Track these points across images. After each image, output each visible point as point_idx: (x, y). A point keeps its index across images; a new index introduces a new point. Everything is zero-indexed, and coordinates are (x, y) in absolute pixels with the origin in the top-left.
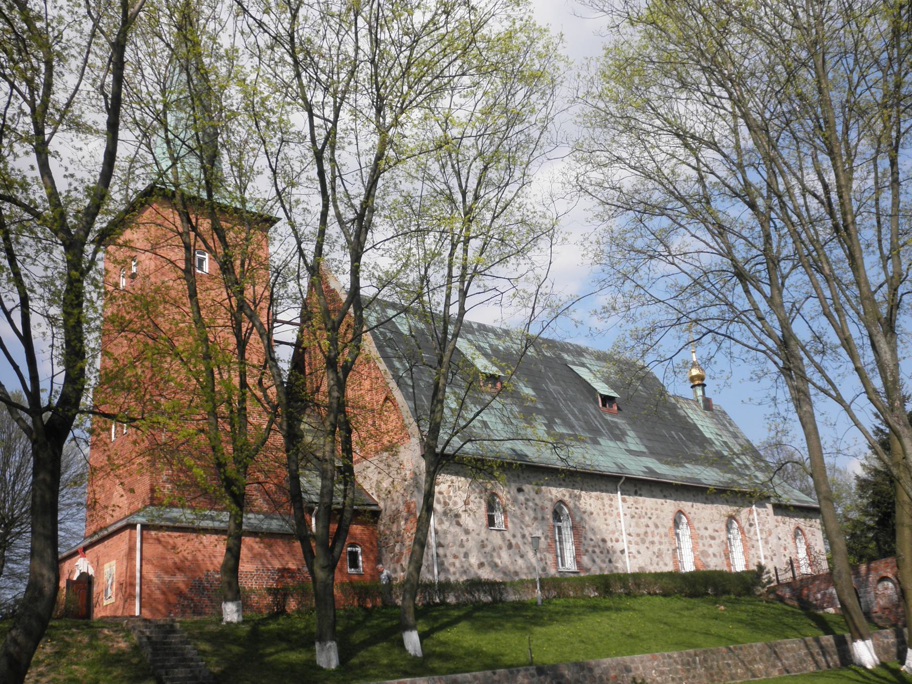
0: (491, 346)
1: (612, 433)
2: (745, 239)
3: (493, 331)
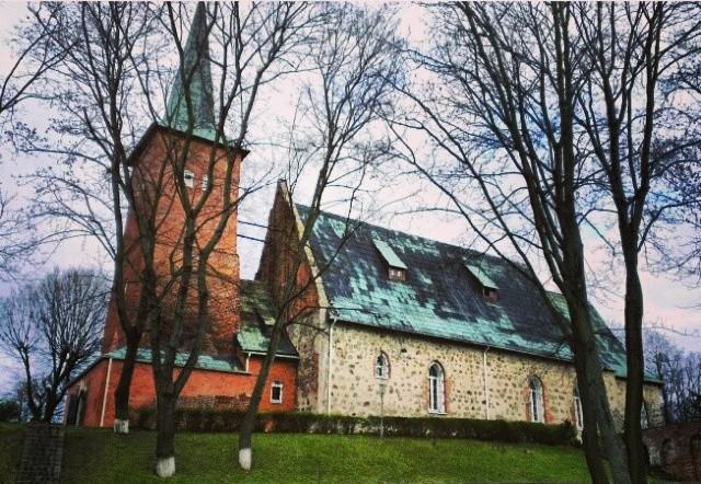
0: (406, 248)
1: (487, 314)
3: (411, 238)
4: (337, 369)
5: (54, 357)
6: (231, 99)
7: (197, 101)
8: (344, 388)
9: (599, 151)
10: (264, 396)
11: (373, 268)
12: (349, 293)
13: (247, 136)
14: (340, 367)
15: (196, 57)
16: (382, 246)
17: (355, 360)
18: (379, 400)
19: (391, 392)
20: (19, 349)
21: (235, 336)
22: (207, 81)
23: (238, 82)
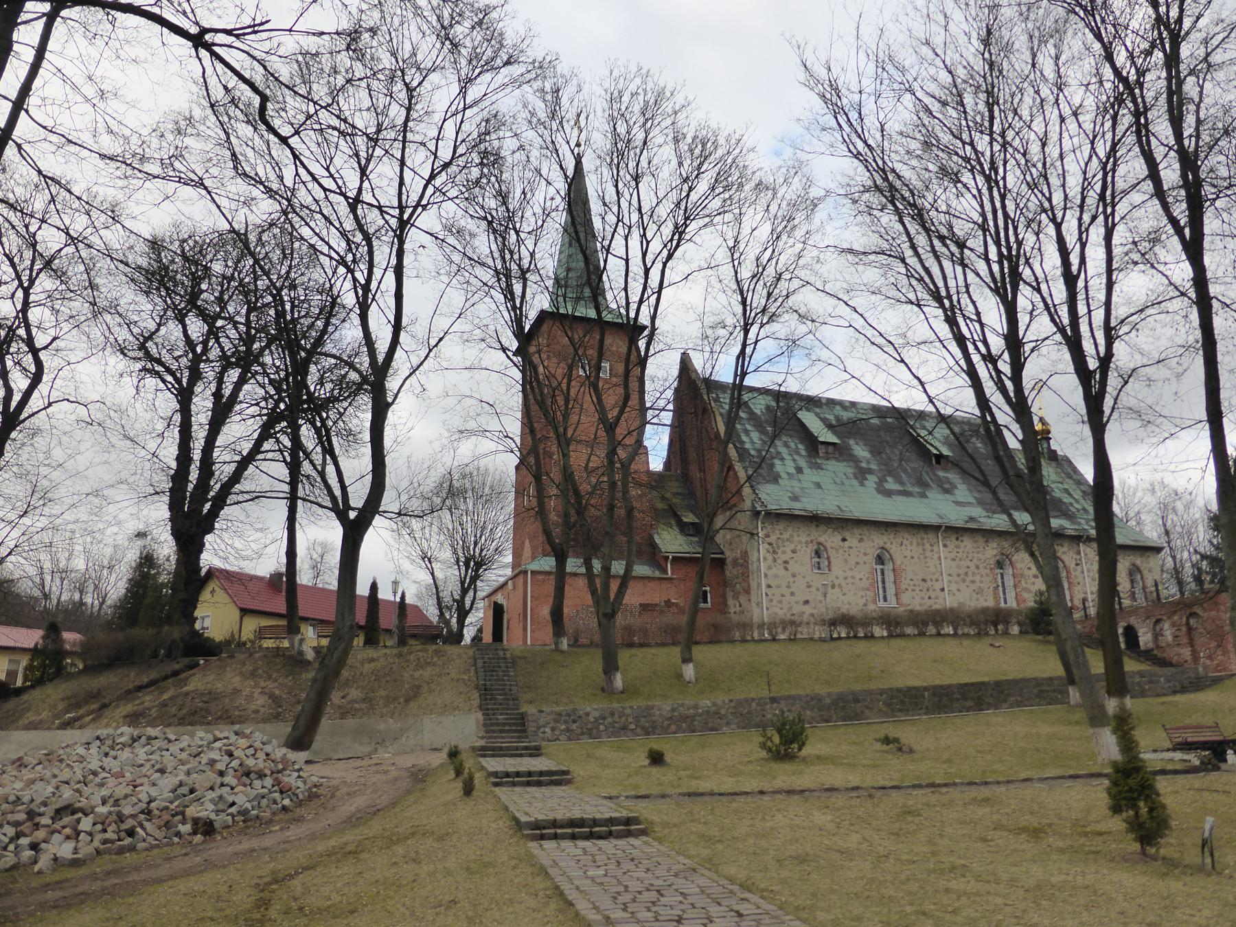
2: (157, 330)
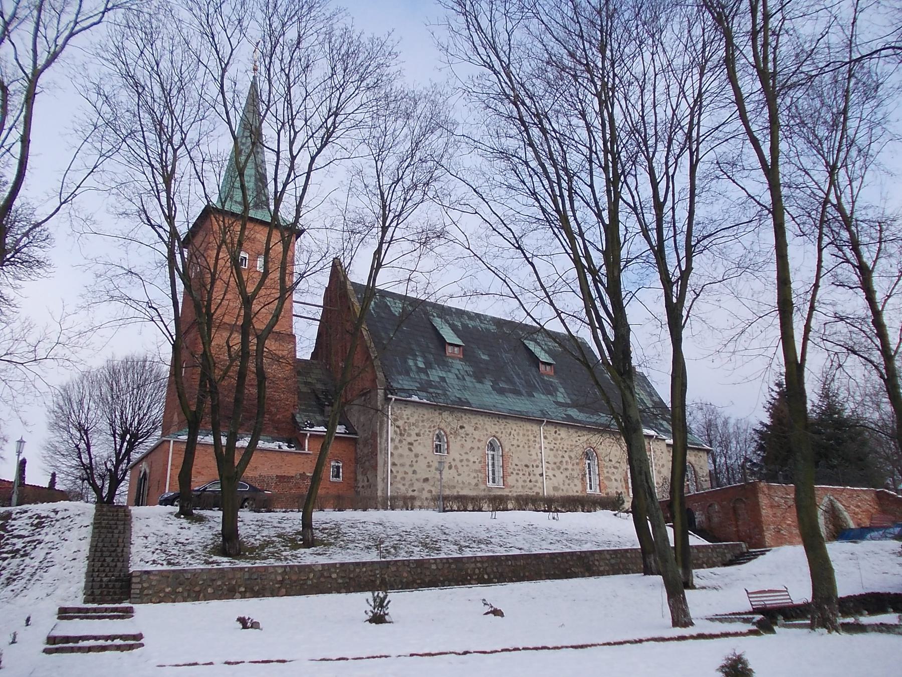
4: (396, 448)
5: (115, 437)
6: (285, 185)
7: (250, 184)
8: (402, 465)
9: (645, 231)
10: (323, 475)
11: (430, 345)
12: (407, 372)
13: (301, 221)
14: (399, 445)
15: (249, 138)
16: (438, 322)
17: (414, 437)
18: (438, 476)
19: (450, 468)
20: (79, 431)
21: (294, 417)
22: (260, 168)
23: (292, 168)
